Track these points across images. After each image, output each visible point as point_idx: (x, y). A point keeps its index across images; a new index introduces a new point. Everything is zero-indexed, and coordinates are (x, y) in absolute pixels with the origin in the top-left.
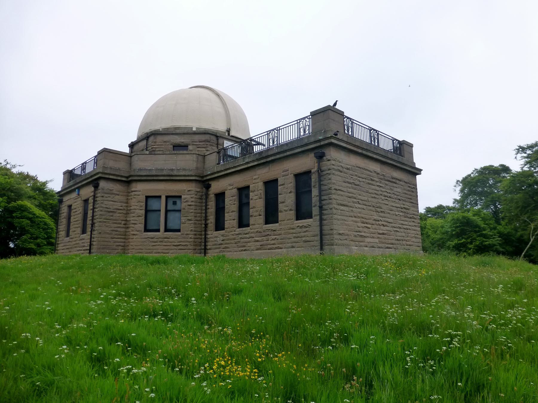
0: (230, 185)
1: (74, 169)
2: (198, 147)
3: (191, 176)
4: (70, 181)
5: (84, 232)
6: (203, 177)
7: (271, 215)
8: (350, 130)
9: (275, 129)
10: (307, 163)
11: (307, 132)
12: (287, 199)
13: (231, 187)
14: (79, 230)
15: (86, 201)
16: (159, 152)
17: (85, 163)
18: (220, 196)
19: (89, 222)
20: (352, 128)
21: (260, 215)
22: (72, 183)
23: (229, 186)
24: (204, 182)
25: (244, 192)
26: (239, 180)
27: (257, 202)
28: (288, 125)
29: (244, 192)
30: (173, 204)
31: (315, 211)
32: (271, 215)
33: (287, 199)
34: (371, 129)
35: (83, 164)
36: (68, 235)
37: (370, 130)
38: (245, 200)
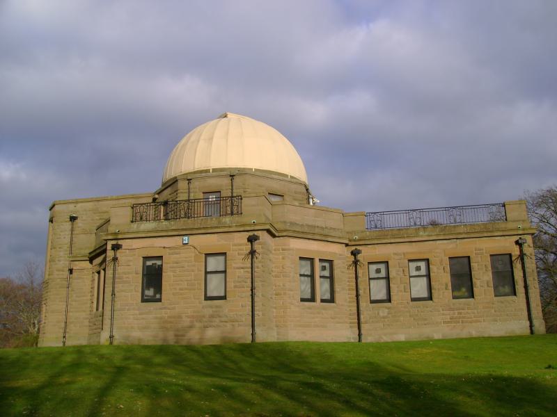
12: (483, 277)
33: (483, 277)
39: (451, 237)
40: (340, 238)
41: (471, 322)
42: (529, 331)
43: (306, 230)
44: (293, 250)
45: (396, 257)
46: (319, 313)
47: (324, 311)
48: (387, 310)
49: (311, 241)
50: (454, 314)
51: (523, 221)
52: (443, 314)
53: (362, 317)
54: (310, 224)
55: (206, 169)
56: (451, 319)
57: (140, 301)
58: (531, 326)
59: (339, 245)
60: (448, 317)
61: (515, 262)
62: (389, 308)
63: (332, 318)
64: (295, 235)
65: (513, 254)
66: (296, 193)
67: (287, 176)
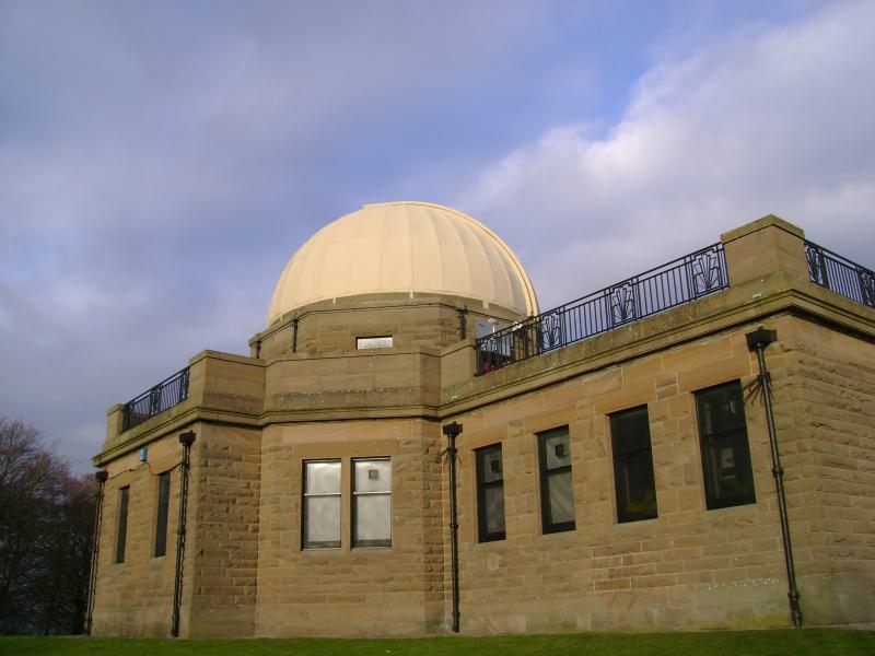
0: (512, 424)
1: (132, 403)
2: (418, 338)
3: (405, 406)
4: (122, 432)
5: (160, 550)
6: (437, 408)
7: (635, 492)
8: (820, 275)
9: (554, 311)
10: (727, 358)
11: (557, 342)
12: (677, 455)
13: (516, 430)
14: (148, 545)
15: (164, 476)
16: (331, 354)
17: (160, 387)
18: (489, 456)
19: (173, 526)
20: (823, 267)
21: (603, 499)
22: (126, 436)
23: (508, 423)
24: (443, 418)
25: (552, 438)
26: (535, 411)
27: (593, 461)
28: (583, 302)
29: (552, 438)
30: (370, 477)
31: (762, 480)
32: (635, 492)
33: (677, 455)
34: (860, 270)
35: (154, 389)
36: (120, 558)
37: (860, 273)
38: (490, 476)
39: (601, 362)
40: (479, 395)
41: (649, 585)
42: (787, 611)
43: (322, 403)
44: (289, 448)
45: (516, 430)
46: (344, 572)
47: (356, 567)
48: (499, 557)
49: (377, 422)
50: (616, 562)
51: (767, 276)
52: (595, 565)
53: (462, 574)
54: (334, 389)
55: (404, 291)
56: (610, 577)
57: (701, 501)
58: (794, 599)
59: (412, 421)
60: (605, 571)
61: (748, 403)
62: (501, 552)
63: (381, 582)
64: (288, 418)
65: (744, 380)
66: (419, 324)
67: (406, 295)
